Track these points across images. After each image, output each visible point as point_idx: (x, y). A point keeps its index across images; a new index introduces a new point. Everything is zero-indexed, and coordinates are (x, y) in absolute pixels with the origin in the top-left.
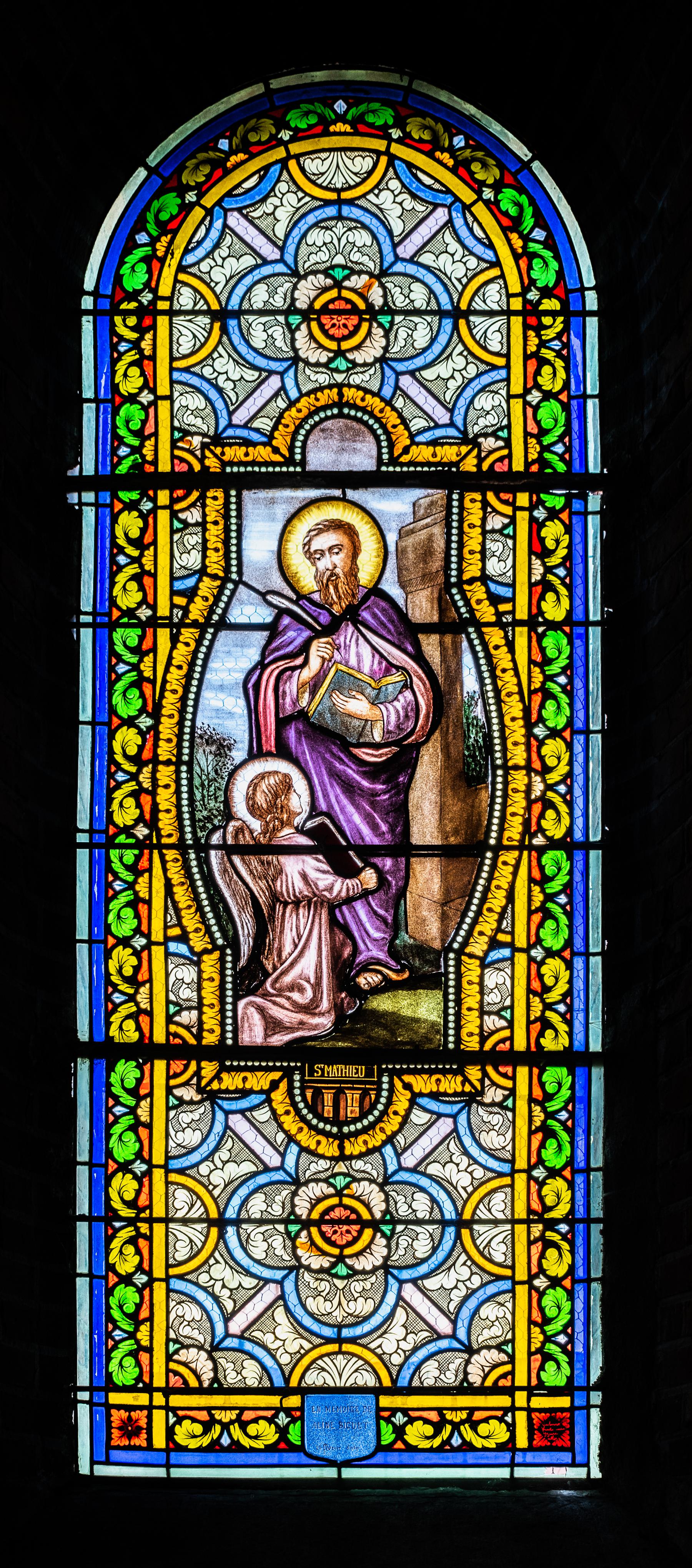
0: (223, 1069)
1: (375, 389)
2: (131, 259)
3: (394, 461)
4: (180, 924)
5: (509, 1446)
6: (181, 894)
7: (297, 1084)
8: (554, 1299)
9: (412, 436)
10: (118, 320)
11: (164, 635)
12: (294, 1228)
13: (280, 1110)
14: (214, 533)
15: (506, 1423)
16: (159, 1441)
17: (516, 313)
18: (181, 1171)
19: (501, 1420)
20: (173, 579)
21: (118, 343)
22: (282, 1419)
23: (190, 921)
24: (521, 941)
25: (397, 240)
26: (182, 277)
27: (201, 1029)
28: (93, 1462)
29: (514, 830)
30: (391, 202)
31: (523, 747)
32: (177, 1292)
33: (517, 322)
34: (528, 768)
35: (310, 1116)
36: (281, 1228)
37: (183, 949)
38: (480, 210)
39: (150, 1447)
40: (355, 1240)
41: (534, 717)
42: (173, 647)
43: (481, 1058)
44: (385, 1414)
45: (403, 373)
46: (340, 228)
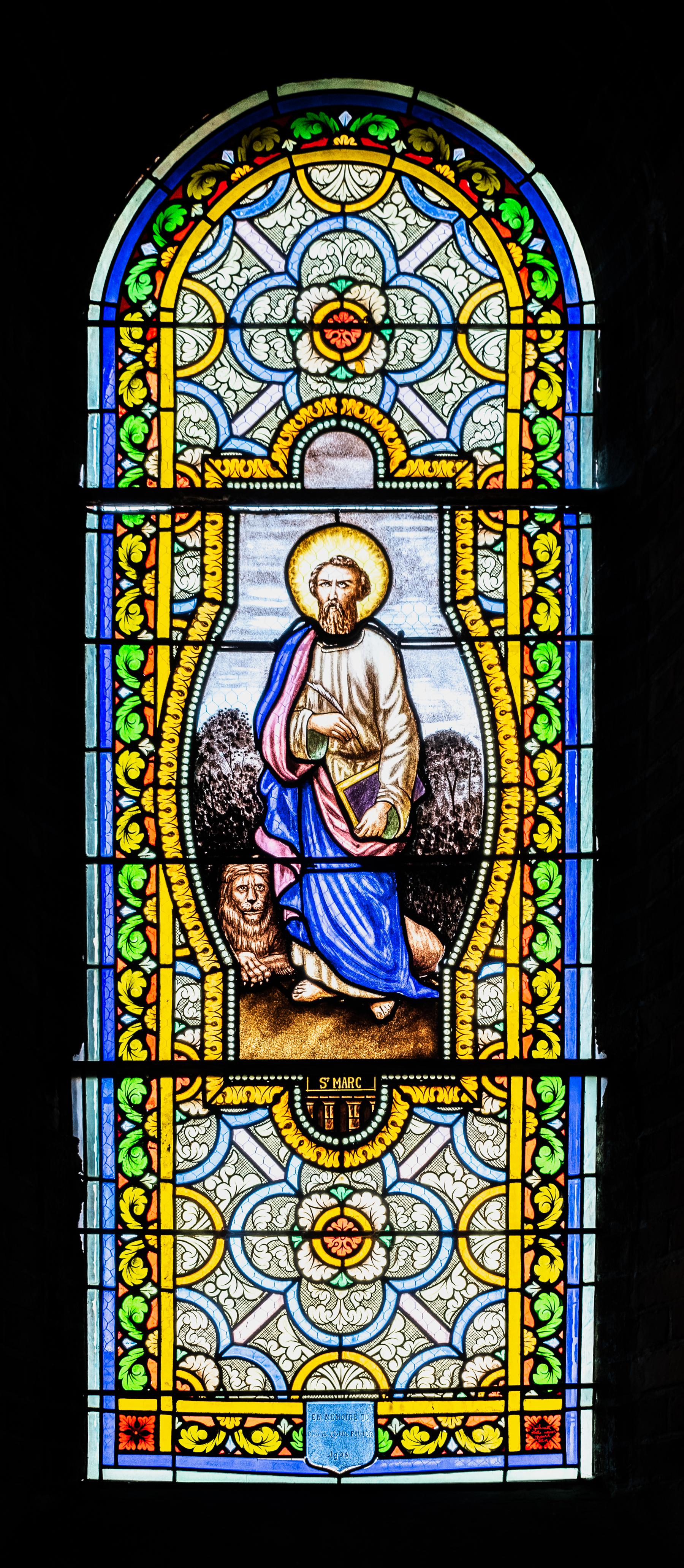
0: (227, 1084)
2: (135, 271)
4: (187, 945)
6: (189, 917)
7: (298, 1098)
9: (408, 450)
10: (123, 331)
14: (212, 559)
17: (516, 327)
18: (189, 1185)
19: (494, 1424)
20: (173, 601)
22: (285, 1426)
23: (198, 940)
24: (513, 956)
25: (400, 254)
26: (187, 283)
27: (203, 1047)
29: (508, 844)
30: (396, 215)
31: (516, 765)
32: (184, 1301)
33: (517, 336)
36: (285, 1239)
37: (487, 605)
40: (355, 1252)
41: (527, 733)
42: (173, 671)
43: (477, 1067)
45: (403, 385)
46: (343, 240)
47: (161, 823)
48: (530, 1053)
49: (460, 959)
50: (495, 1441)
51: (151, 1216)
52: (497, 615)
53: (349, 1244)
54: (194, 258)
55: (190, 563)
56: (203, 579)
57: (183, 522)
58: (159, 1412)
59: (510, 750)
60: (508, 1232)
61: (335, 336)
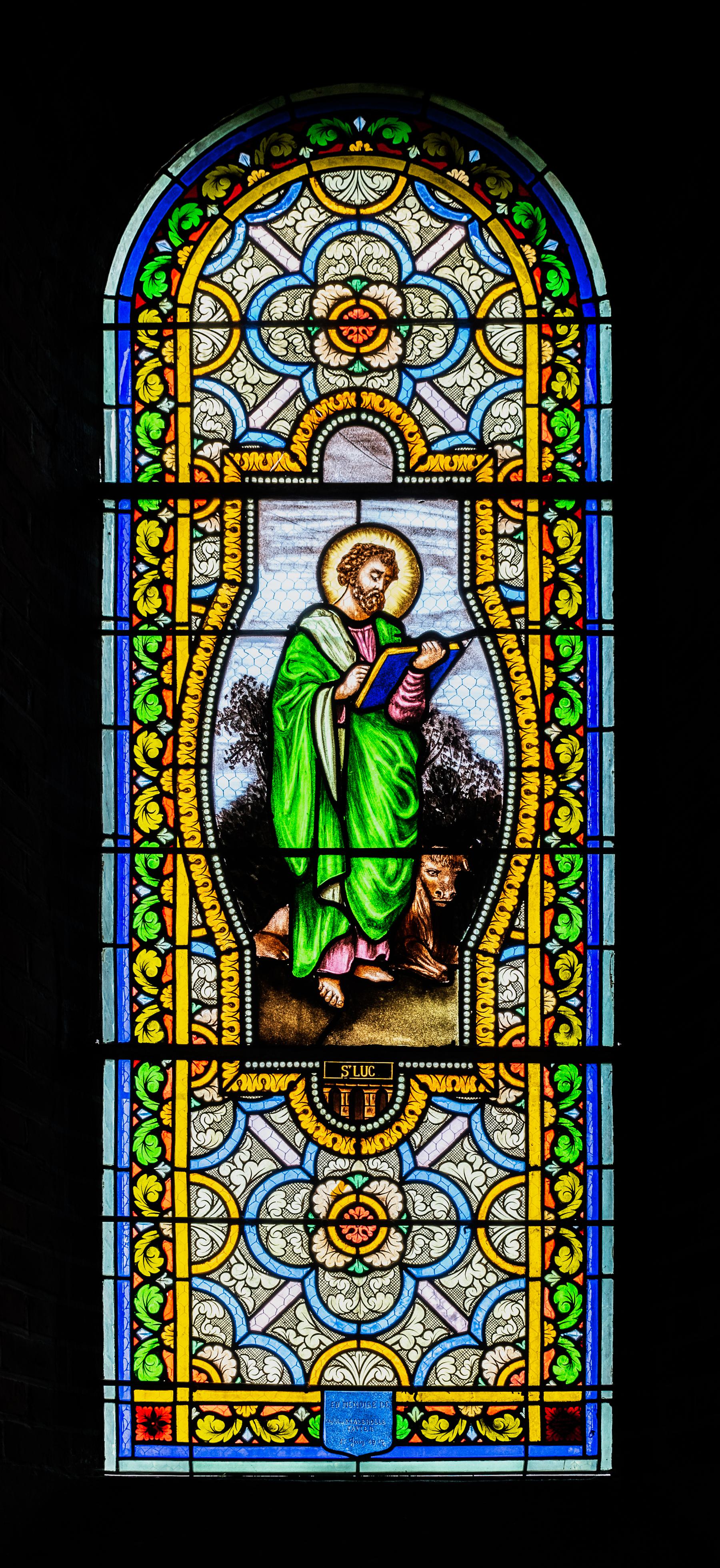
0: (242, 1070)
1: (393, 395)
3: (410, 472)
4: (204, 925)
5: (523, 1439)
6: (207, 898)
8: (564, 1294)
9: (429, 445)
11: (182, 643)
12: (313, 330)
13: (299, 1109)
14: (231, 538)
15: (521, 1417)
16: (183, 1435)
17: (532, 321)
19: (515, 1414)
20: (191, 587)
21: (139, 351)
23: (215, 919)
24: (534, 937)
26: (203, 285)
27: (220, 1028)
28: (119, 1458)
29: (527, 829)
30: (410, 220)
33: (532, 330)
34: (542, 771)
35: (328, 1117)
38: (494, 225)
39: (174, 1442)
40: (371, 1240)
43: (495, 1055)
44: (401, 1408)
46: (359, 241)
47: (180, 803)
48: (551, 1036)
49: (479, 942)
50: (516, 1431)
51: (166, 1204)
52: (516, 604)
53: (364, 1232)
54: (209, 260)
55: (210, 547)
56: (222, 562)
57: (201, 508)
58: (175, 1403)
59: (530, 736)
60: (527, 1223)
61: (351, 332)
